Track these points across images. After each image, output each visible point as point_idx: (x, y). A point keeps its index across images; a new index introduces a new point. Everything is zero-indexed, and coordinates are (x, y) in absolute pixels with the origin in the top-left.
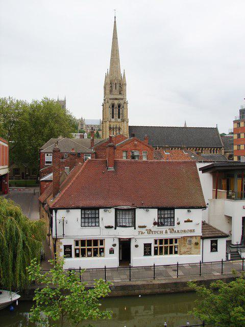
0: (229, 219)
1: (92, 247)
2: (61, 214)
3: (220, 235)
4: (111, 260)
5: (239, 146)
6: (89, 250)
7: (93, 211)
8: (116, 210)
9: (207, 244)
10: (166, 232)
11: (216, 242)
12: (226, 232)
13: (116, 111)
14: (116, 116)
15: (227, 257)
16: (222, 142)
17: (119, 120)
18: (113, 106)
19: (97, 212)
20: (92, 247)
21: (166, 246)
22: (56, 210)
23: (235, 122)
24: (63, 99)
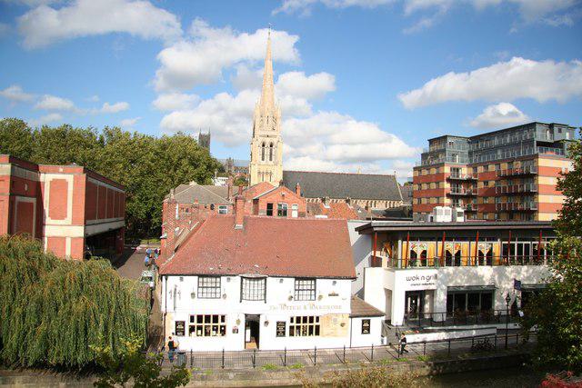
0: (389, 293)
1: (209, 324)
2: (173, 280)
3: (374, 313)
4: (235, 342)
5: (420, 199)
6: (200, 328)
7: (214, 280)
8: (242, 278)
9: (358, 322)
10: (305, 308)
11: (369, 322)
12: (382, 308)
13: (267, 151)
14: (267, 158)
15: (382, 341)
16: (34, 213)
17: (271, 163)
18: (263, 146)
19: (218, 279)
20: (209, 324)
21: (308, 325)
22: (167, 276)
23: (415, 169)
24: (207, 133)
